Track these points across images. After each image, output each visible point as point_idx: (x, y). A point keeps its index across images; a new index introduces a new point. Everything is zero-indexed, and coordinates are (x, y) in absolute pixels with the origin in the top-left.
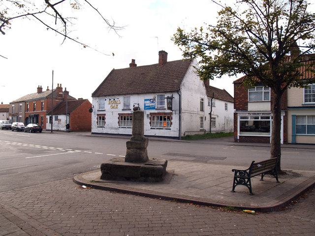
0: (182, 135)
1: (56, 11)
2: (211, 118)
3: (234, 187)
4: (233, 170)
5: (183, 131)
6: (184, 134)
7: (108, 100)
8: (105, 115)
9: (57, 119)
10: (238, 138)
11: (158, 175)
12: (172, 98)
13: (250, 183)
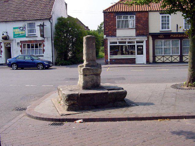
10: (109, 61)
11: (118, 99)
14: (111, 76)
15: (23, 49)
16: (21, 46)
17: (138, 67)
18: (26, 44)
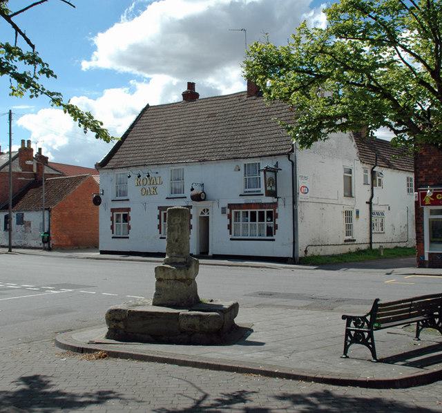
0: (301, 254)
1: (15, 26)
2: (371, 213)
3: (346, 347)
4: (344, 317)
5: (303, 242)
6: (306, 251)
7: (134, 177)
8: (128, 210)
9: (20, 221)
10: (427, 258)
11: (223, 328)
12: (275, 170)
13: (373, 340)
14: (214, 284)
15: (115, 224)
16: (230, 217)
17: (215, 265)
18: (241, 211)
